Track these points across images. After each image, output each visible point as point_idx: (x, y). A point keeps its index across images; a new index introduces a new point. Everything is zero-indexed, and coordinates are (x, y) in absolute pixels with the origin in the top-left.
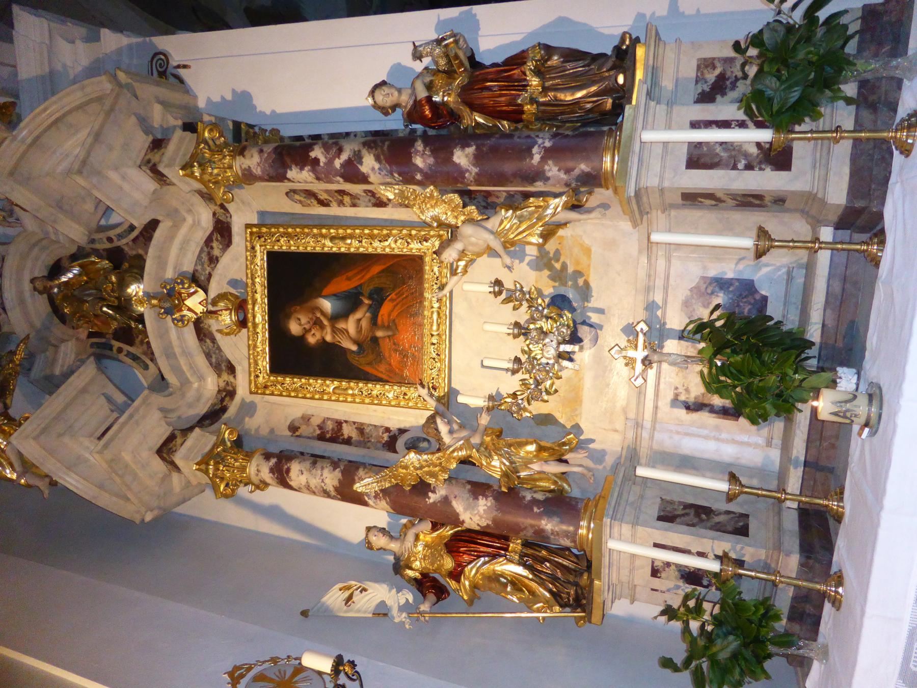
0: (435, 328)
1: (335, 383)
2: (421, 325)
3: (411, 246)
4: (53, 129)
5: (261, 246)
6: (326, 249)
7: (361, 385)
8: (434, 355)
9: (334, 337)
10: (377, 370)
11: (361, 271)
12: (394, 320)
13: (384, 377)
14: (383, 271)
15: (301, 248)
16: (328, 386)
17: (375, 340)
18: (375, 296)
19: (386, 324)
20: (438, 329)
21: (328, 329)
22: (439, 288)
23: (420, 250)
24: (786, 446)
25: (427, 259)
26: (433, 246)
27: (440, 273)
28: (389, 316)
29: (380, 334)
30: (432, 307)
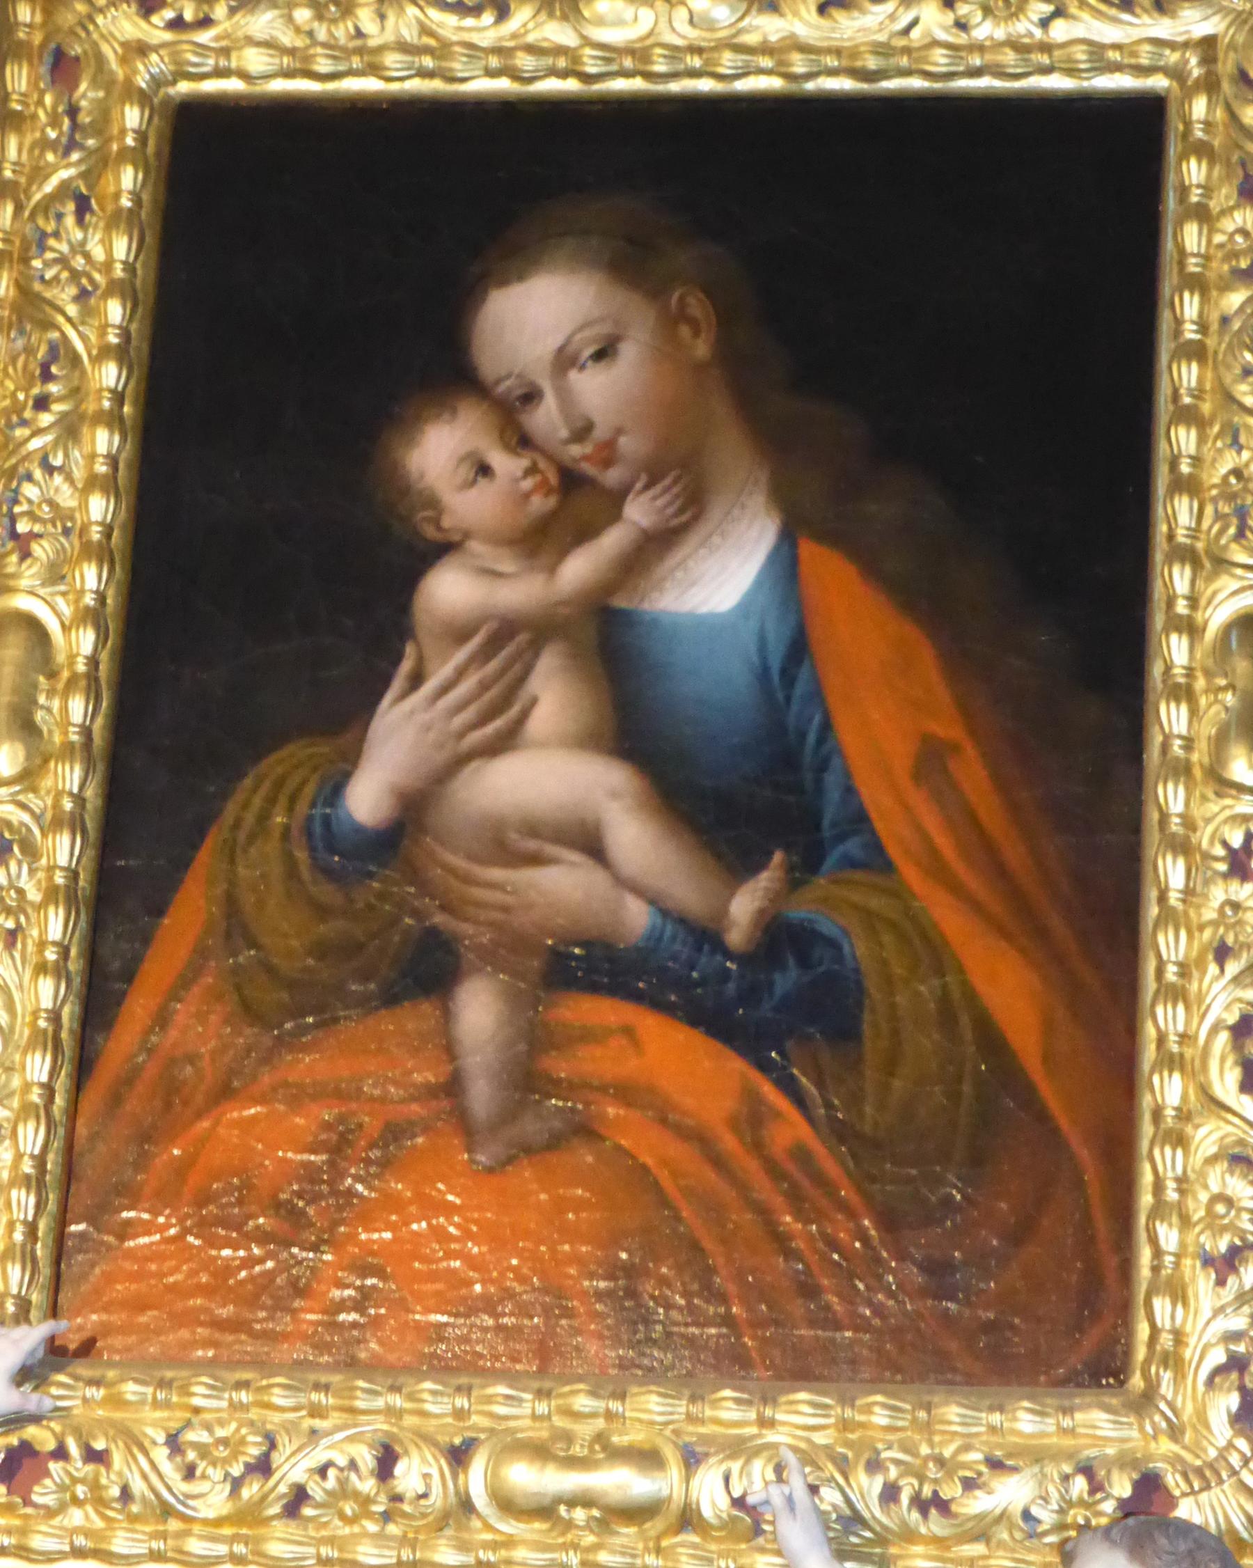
0: (526, 1477)
1: (86, 640)
2: (546, 1361)
3: (1202, 1284)
4: (73, 1181)
5: (1208, 45)
6: (1180, 579)
7: (63, 849)
8: (294, 1468)
9: (461, 634)
10: (185, 982)
11: (999, 871)
12: (585, 1130)
13: (123, 1043)
14: (991, 1041)
15: (1189, 374)
16: (55, 574)
17: (429, 971)
18: (786, 980)
19: (560, 1067)
20: (507, 1504)
21: (521, 591)
22: (854, 1519)
23: (1173, 1360)
24: (268, 77)
25: (1099, 1425)
26: (1204, 1476)
27: (981, 1530)
28: (625, 1093)
29: (479, 1010)
30: (692, 1460)
